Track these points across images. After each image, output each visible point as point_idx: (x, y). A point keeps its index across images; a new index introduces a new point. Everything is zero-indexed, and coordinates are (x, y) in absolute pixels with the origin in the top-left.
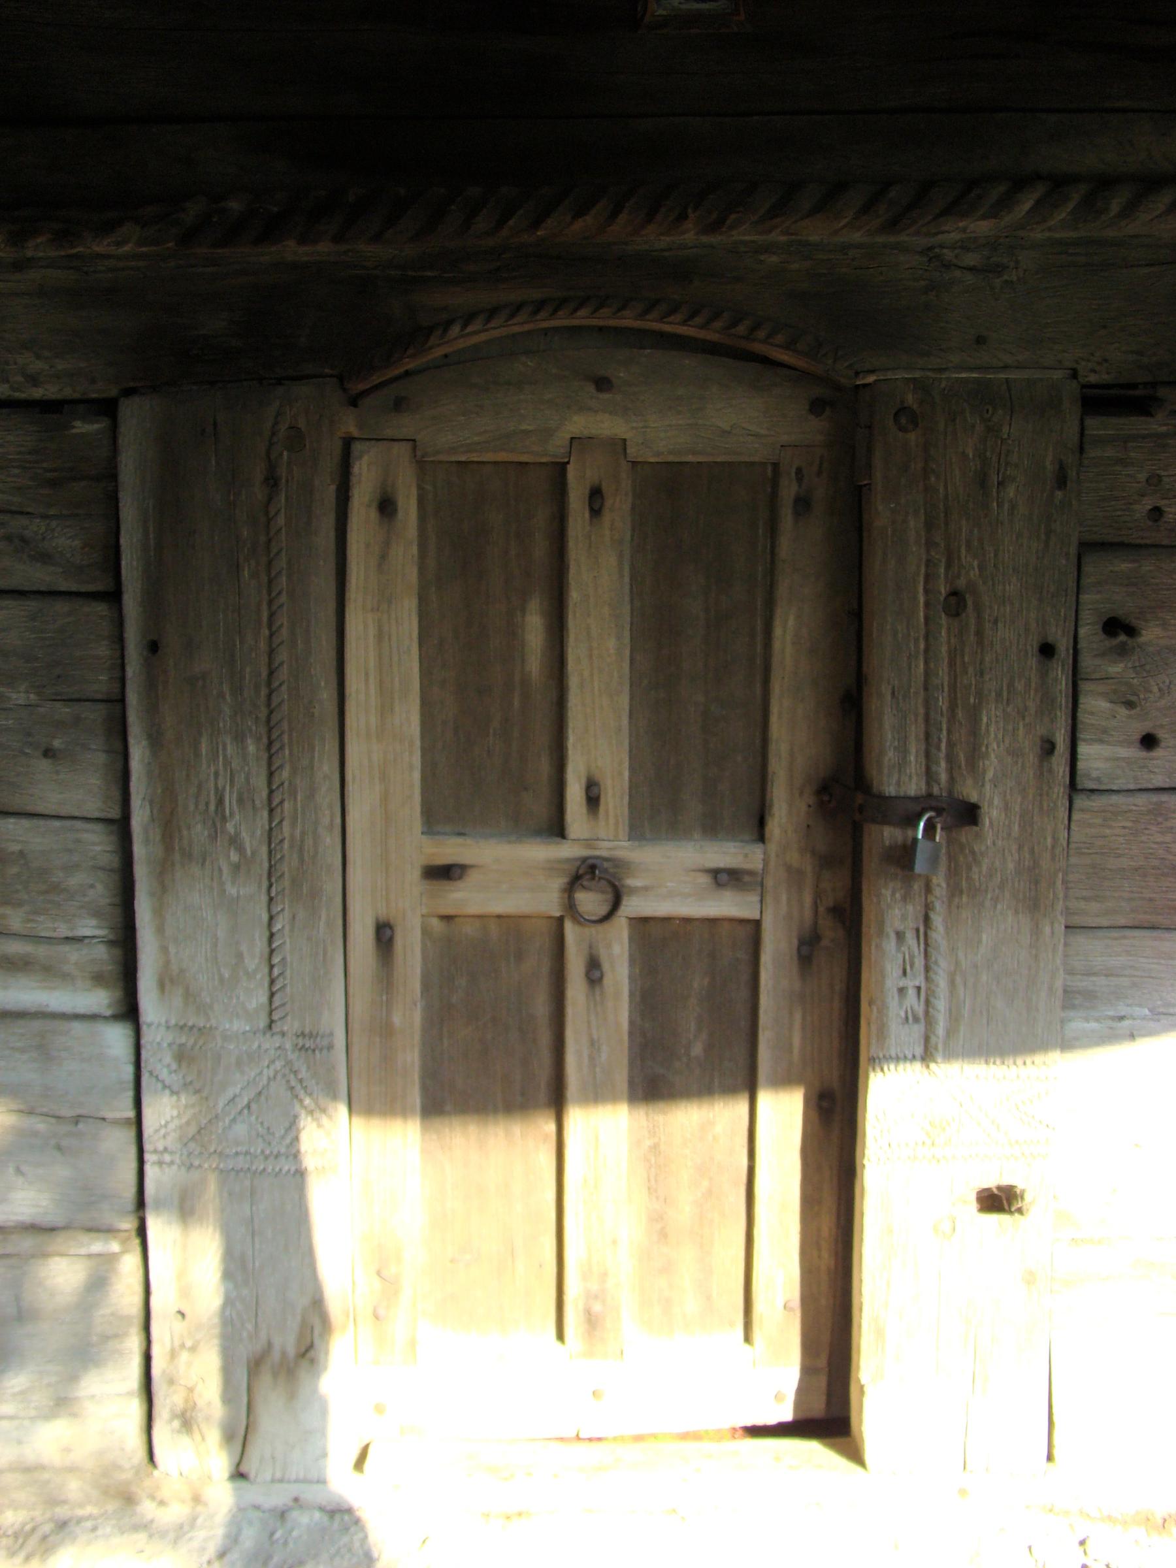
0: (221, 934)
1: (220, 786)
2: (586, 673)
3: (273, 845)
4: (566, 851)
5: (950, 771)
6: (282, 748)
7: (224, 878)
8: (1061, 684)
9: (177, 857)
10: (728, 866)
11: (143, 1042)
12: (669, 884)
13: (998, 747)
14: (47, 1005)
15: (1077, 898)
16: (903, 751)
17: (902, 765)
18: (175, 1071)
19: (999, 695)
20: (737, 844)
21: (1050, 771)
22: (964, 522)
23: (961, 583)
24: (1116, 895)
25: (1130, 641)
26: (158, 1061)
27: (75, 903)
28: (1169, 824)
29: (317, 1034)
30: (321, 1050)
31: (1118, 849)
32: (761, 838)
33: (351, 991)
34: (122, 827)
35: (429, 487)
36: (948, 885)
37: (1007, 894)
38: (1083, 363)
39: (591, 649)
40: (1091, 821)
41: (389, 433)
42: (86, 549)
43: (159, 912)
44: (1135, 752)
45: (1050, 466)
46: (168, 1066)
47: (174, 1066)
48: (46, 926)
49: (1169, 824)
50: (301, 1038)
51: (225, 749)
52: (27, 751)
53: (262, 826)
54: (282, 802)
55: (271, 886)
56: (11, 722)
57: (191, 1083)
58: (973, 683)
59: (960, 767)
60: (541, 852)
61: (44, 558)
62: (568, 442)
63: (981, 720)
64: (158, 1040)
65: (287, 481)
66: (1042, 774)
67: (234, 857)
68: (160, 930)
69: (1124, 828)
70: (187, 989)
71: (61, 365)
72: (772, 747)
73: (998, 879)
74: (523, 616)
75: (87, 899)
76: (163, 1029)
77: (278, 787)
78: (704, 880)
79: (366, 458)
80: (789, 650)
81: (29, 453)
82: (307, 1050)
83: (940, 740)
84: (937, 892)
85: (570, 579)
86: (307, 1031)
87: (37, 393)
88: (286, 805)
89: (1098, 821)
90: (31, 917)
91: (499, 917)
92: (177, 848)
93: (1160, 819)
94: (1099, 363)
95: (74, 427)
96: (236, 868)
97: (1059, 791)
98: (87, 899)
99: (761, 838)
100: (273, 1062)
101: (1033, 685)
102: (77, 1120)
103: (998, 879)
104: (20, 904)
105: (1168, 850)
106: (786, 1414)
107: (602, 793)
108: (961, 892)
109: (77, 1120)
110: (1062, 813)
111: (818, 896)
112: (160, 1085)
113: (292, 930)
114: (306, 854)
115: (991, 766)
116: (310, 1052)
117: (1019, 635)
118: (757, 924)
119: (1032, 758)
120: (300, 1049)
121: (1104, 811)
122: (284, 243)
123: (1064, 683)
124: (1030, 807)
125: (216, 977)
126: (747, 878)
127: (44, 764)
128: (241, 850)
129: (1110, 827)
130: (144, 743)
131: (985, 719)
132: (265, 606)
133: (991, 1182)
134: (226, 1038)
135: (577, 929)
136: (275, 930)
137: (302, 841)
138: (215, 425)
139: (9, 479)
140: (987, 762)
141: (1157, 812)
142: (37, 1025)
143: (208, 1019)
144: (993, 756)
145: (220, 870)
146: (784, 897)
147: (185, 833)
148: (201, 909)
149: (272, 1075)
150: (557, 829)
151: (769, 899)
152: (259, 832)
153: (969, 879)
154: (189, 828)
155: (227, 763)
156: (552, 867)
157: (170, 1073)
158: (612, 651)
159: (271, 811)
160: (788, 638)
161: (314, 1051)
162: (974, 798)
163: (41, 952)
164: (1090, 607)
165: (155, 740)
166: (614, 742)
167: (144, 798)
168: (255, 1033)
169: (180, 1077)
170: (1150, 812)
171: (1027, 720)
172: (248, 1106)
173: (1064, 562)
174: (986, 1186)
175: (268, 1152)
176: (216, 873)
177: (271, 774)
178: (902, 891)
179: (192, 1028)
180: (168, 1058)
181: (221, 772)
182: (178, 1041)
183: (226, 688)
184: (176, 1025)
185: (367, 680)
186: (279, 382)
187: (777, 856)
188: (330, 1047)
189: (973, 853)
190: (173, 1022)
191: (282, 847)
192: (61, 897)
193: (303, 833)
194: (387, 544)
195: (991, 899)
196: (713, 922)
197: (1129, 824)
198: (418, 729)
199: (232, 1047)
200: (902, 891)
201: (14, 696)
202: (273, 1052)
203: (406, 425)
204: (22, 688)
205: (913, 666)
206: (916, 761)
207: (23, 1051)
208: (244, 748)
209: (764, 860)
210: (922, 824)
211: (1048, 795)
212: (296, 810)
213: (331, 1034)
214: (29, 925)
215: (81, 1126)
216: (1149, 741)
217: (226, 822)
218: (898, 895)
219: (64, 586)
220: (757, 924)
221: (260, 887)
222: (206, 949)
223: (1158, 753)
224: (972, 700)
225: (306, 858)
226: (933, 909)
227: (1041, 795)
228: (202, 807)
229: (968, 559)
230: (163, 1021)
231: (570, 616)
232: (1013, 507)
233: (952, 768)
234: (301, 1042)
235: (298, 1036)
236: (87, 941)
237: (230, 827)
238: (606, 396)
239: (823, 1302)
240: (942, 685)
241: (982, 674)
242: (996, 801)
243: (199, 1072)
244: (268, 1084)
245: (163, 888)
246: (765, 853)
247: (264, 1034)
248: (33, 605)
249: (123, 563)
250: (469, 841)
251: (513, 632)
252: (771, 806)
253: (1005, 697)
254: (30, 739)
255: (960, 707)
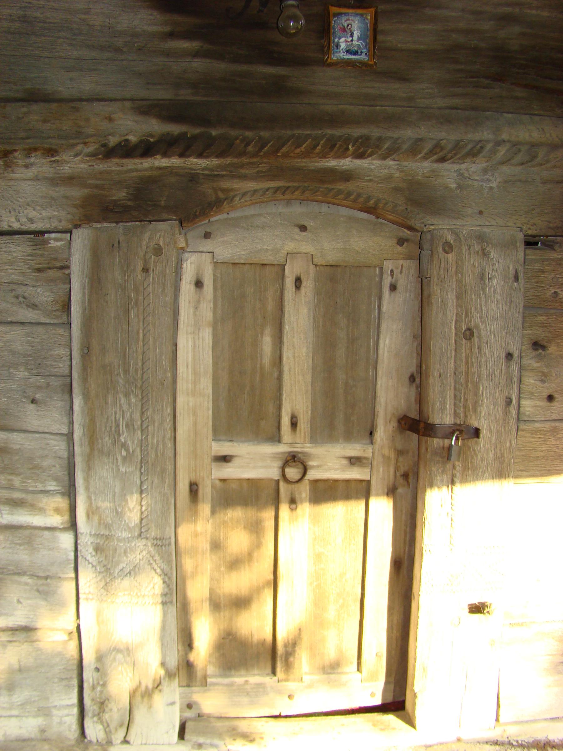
0: (117, 490)
1: (117, 418)
2: (292, 365)
3: (143, 448)
4: (282, 448)
5: (465, 413)
6: (148, 400)
7: (119, 464)
8: (515, 372)
9: (96, 453)
10: (356, 455)
11: (79, 542)
12: (329, 464)
13: (487, 401)
14: (32, 523)
15: (518, 470)
16: (444, 403)
17: (444, 409)
18: (94, 556)
19: (488, 376)
20: (361, 445)
21: (510, 412)
22: (473, 296)
23: (472, 325)
24: (534, 468)
25: (543, 353)
26: (87, 551)
27: (46, 474)
28: (559, 436)
29: (163, 538)
30: (165, 546)
31: (537, 447)
32: (372, 443)
33: (178, 515)
34: (70, 437)
35: (218, 275)
36: (462, 465)
37: (489, 469)
38: (526, 225)
39: (294, 353)
40: (526, 435)
41: (201, 249)
42: (54, 303)
43: (87, 480)
44: (544, 403)
45: (512, 272)
46: (91, 553)
47: (94, 553)
48: (32, 485)
49: (559, 436)
50: (155, 540)
51: (120, 401)
52: (24, 400)
53: (138, 438)
54: (148, 427)
55: (141, 467)
56: (15, 386)
57: (102, 561)
58: (476, 371)
59: (469, 411)
60: (269, 449)
61: (34, 306)
62: (286, 255)
63: (480, 388)
64: (86, 541)
65: (153, 270)
66: (506, 414)
67: (124, 453)
68: (87, 488)
69: (540, 438)
70: (100, 517)
71: (44, 213)
72: (378, 400)
73: (484, 463)
74: (262, 338)
75: (52, 472)
76: (88, 536)
77: (146, 419)
78: (345, 462)
79: (189, 261)
80: (386, 354)
81: (28, 256)
82: (158, 546)
83: (461, 398)
84: (458, 468)
85: (285, 320)
86: (158, 537)
87: (33, 227)
88: (150, 428)
89: (529, 435)
90: (25, 481)
91: (248, 479)
92: (96, 448)
93: (555, 434)
94: (532, 226)
95: (50, 243)
96: (124, 458)
97: (513, 421)
98: (52, 472)
99: (372, 443)
100: (142, 552)
101: (503, 373)
102: (47, 578)
103: (484, 463)
104: (18, 474)
105: (558, 448)
106: (377, 701)
107: (298, 422)
108: (469, 469)
109: (47, 578)
110: (514, 431)
111: (397, 469)
112: (87, 562)
113: (152, 488)
114: (159, 452)
115: (484, 410)
116: (159, 547)
117: (497, 349)
118: (369, 482)
119: (502, 406)
120: (155, 546)
121: (532, 431)
122: (155, 156)
123: (516, 371)
124: (500, 429)
125: (115, 511)
126: (364, 461)
127: (32, 407)
128: (127, 450)
129: (533, 437)
130: (81, 397)
131: (481, 388)
132: (141, 331)
133: (476, 601)
134: (119, 540)
135: (286, 485)
136: (143, 488)
137: (157, 445)
138: (119, 242)
139: (18, 268)
140: (481, 408)
141: (554, 430)
142: (27, 532)
143: (111, 531)
144: (484, 405)
145: (117, 459)
146: (381, 469)
147: (100, 441)
148: (107, 478)
149: (141, 558)
150: (276, 438)
151: (374, 471)
152: (136, 442)
153: (472, 462)
154: (102, 439)
155: (121, 407)
156: (275, 456)
157: (92, 556)
158: (304, 354)
159: (142, 431)
160: (386, 349)
161: (162, 546)
162: (475, 424)
163: (29, 497)
164: (527, 336)
165: (86, 396)
166: (304, 397)
167: (80, 424)
168: (133, 538)
169: (97, 559)
170: (551, 431)
171: (500, 389)
172: (130, 573)
173: (517, 316)
174: (473, 602)
175: (139, 594)
176: (115, 461)
177: (142, 413)
178: (442, 469)
179: (103, 535)
180: (91, 550)
181: (118, 412)
182: (96, 542)
183: (121, 371)
184: (95, 534)
185: (187, 367)
186: (150, 221)
187: (379, 450)
188: (170, 544)
189: (474, 450)
190: (93, 532)
191: (147, 448)
192: (39, 471)
193: (158, 442)
194: (198, 302)
195: (482, 472)
196: (347, 481)
197: (542, 436)
198: (211, 390)
199: (122, 544)
200: (442, 469)
201: (18, 373)
202: (142, 547)
203: (208, 245)
204: (21, 370)
205: (449, 364)
206: (450, 408)
207: (20, 545)
208: (129, 400)
209: (372, 453)
210: (454, 438)
211: (508, 423)
212: (154, 430)
213: (170, 538)
214: (23, 484)
215: (48, 580)
216: (550, 398)
217: (120, 436)
218: (440, 470)
219: (43, 320)
220: (369, 482)
221: (136, 468)
222: (110, 498)
223: (555, 403)
224: (475, 379)
225: (159, 454)
226: (456, 477)
227: (505, 424)
228: (108, 429)
229: (475, 313)
230: (88, 532)
231: (285, 338)
232: (495, 291)
233: (465, 411)
234: (155, 542)
235: (154, 540)
236: (51, 492)
237: (122, 439)
238: (304, 234)
239: (393, 652)
240: (462, 372)
241: (480, 367)
242: (485, 427)
243: (106, 557)
244: (139, 562)
245: (89, 468)
246: (373, 449)
247: (138, 538)
248: (27, 329)
249: (72, 309)
250: (235, 444)
251: (256, 344)
252: (376, 427)
253: (490, 378)
254: (25, 395)
255: (470, 382)
